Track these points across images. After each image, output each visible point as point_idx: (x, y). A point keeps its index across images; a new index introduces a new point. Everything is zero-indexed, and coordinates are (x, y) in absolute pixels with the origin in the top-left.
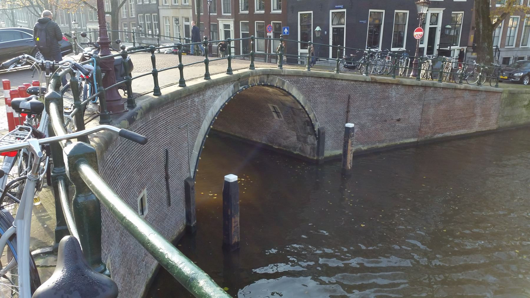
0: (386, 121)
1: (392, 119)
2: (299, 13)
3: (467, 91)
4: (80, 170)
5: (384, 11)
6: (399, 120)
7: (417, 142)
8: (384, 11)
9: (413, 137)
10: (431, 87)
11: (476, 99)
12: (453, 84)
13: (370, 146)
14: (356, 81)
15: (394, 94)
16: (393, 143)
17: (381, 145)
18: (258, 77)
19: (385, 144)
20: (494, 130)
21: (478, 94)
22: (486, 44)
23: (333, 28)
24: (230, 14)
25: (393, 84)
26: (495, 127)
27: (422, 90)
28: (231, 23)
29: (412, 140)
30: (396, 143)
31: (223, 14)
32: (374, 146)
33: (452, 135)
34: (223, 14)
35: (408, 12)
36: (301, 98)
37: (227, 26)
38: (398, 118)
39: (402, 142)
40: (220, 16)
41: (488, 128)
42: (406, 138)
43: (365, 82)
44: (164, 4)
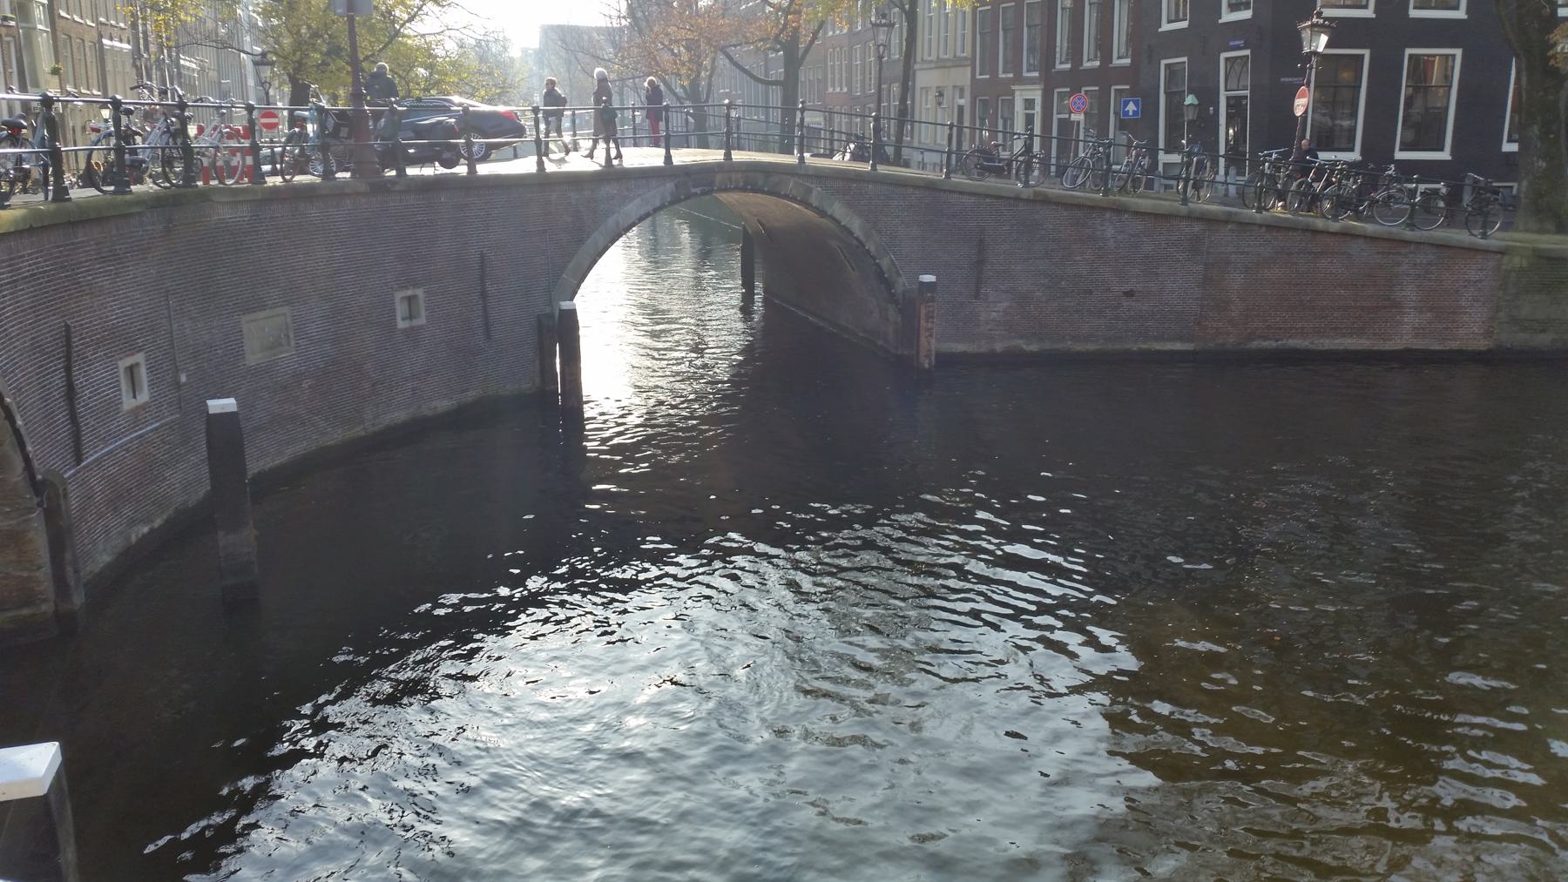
0: (1091, 292)
1: (1108, 290)
2: (1164, 62)
3: (1361, 241)
4: (660, 434)
5: (1366, 53)
6: (1129, 294)
7: (1194, 353)
8: (1366, 53)
9: (1181, 339)
10: (1227, 222)
11: (1399, 264)
12: (1306, 218)
13: (1047, 346)
14: (999, 197)
15: (1110, 232)
16: (1118, 346)
17: (1079, 347)
18: (739, 175)
19: (1091, 347)
20: (1480, 353)
21: (1403, 251)
22: (1536, 129)
23: (1228, 98)
24: (1036, 74)
25: (1105, 209)
26: (1482, 344)
27: (1197, 227)
28: (1037, 95)
29: (1178, 346)
30: (1128, 346)
31: (1026, 74)
32: (1059, 346)
33: (1312, 347)
34: (1026, 74)
35: (1458, 52)
36: (856, 225)
37: (1029, 104)
38: (1127, 288)
39: (1144, 346)
40: (1019, 79)
41: (1454, 345)
42: (1157, 339)
43: (1017, 199)
44: (926, 58)
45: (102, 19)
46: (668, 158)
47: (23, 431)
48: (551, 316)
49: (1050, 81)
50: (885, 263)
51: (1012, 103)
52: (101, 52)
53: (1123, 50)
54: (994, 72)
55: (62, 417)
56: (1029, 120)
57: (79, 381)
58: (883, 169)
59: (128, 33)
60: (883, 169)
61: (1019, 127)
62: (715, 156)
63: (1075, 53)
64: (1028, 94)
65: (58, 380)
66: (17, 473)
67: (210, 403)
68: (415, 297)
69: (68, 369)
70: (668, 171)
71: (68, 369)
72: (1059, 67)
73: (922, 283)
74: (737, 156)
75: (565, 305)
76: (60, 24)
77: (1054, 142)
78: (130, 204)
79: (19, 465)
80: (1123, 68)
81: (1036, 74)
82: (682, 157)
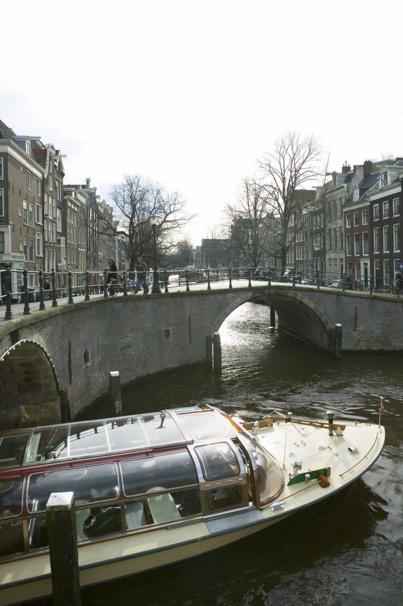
24: (368, 255)
31: (364, 255)
34: (364, 255)
37: (366, 264)
45: (79, 243)
46: (209, 287)
47: (57, 375)
48: (210, 336)
49: (372, 257)
50: (323, 319)
51: (359, 264)
52: (78, 252)
53: (377, 250)
54: (353, 254)
55: (67, 370)
56: (366, 270)
57: (72, 358)
58: (321, 288)
59: (85, 246)
60: (321, 288)
61: (363, 273)
62: (265, 283)
63: (380, 248)
64: (365, 262)
65: (66, 359)
66: (54, 389)
67: (112, 373)
68: (169, 330)
69: (69, 355)
70: (250, 288)
71: (69, 355)
72: (375, 253)
73: (336, 327)
74: (273, 284)
75: (216, 333)
76: (68, 244)
77: (265, 283)
78: (89, 303)
79: (55, 385)
80: (398, 253)
81: (368, 255)
82: (255, 283)
